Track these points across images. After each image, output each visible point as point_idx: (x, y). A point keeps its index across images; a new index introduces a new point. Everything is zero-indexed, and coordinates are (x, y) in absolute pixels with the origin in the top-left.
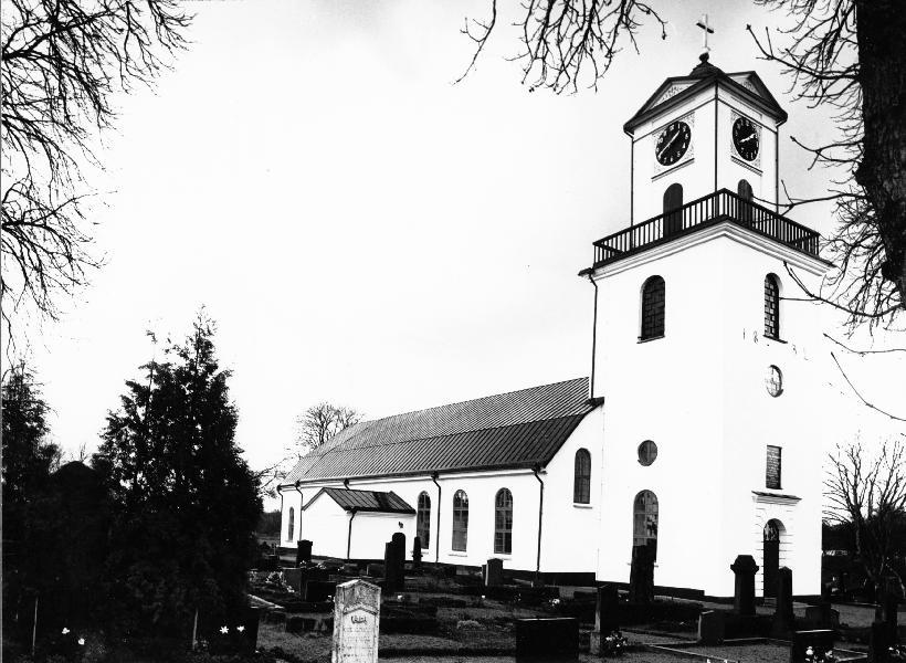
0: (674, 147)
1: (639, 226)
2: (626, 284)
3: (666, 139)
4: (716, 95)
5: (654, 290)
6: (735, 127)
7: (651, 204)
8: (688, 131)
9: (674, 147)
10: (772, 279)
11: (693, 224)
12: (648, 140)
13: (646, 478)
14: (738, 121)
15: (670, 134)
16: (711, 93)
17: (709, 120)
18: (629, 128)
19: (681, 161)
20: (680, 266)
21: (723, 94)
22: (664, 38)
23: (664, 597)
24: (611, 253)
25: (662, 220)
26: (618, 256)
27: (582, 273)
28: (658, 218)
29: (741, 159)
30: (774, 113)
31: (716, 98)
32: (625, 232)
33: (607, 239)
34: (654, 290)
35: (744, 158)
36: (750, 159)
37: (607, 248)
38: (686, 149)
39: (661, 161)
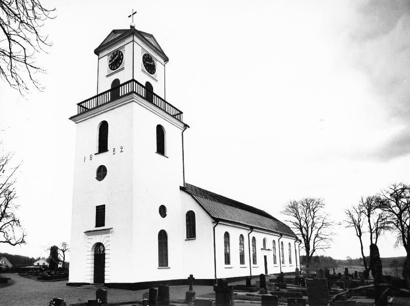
0: (116, 62)
1: (101, 94)
2: (92, 126)
3: (113, 58)
4: (133, 39)
5: (104, 127)
6: (144, 57)
7: (107, 85)
8: (122, 55)
9: (116, 62)
10: (160, 131)
11: (125, 93)
12: (105, 61)
13: (101, 193)
14: (145, 55)
15: (114, 56)
16: (130, 39)
17: (133, 52)
18: (97, 52)
19: (118, 69)
20: (115, 117)
21: (136, 38)
22: (289, 243)
23: (127, 35)
24: (84, 111)
25: (109, 93)
26: (87, 110)
27: (71, 118)
28: (108, 91)
29: (147, 72)
30: (128, 34)
31: (133, 41)
32: (93, 98)
33: (83, 102)
34: (104, 127)
35: (148, 71)
36: (152, 74)
37: (83, 107)
38: (123, 58)
39: (111, 69)
